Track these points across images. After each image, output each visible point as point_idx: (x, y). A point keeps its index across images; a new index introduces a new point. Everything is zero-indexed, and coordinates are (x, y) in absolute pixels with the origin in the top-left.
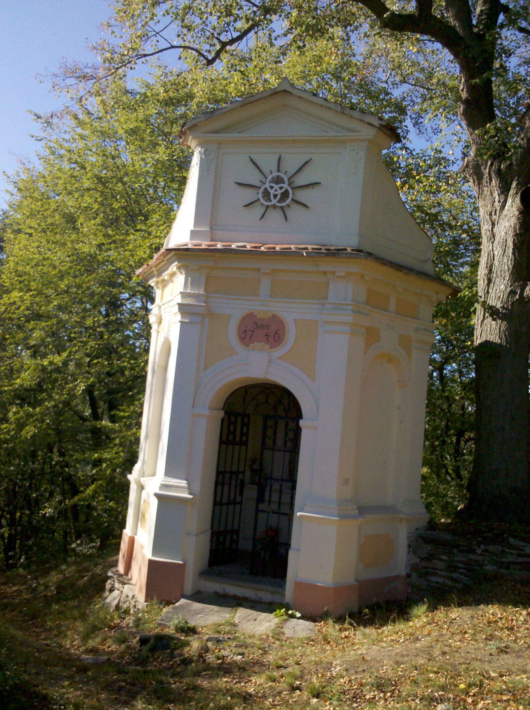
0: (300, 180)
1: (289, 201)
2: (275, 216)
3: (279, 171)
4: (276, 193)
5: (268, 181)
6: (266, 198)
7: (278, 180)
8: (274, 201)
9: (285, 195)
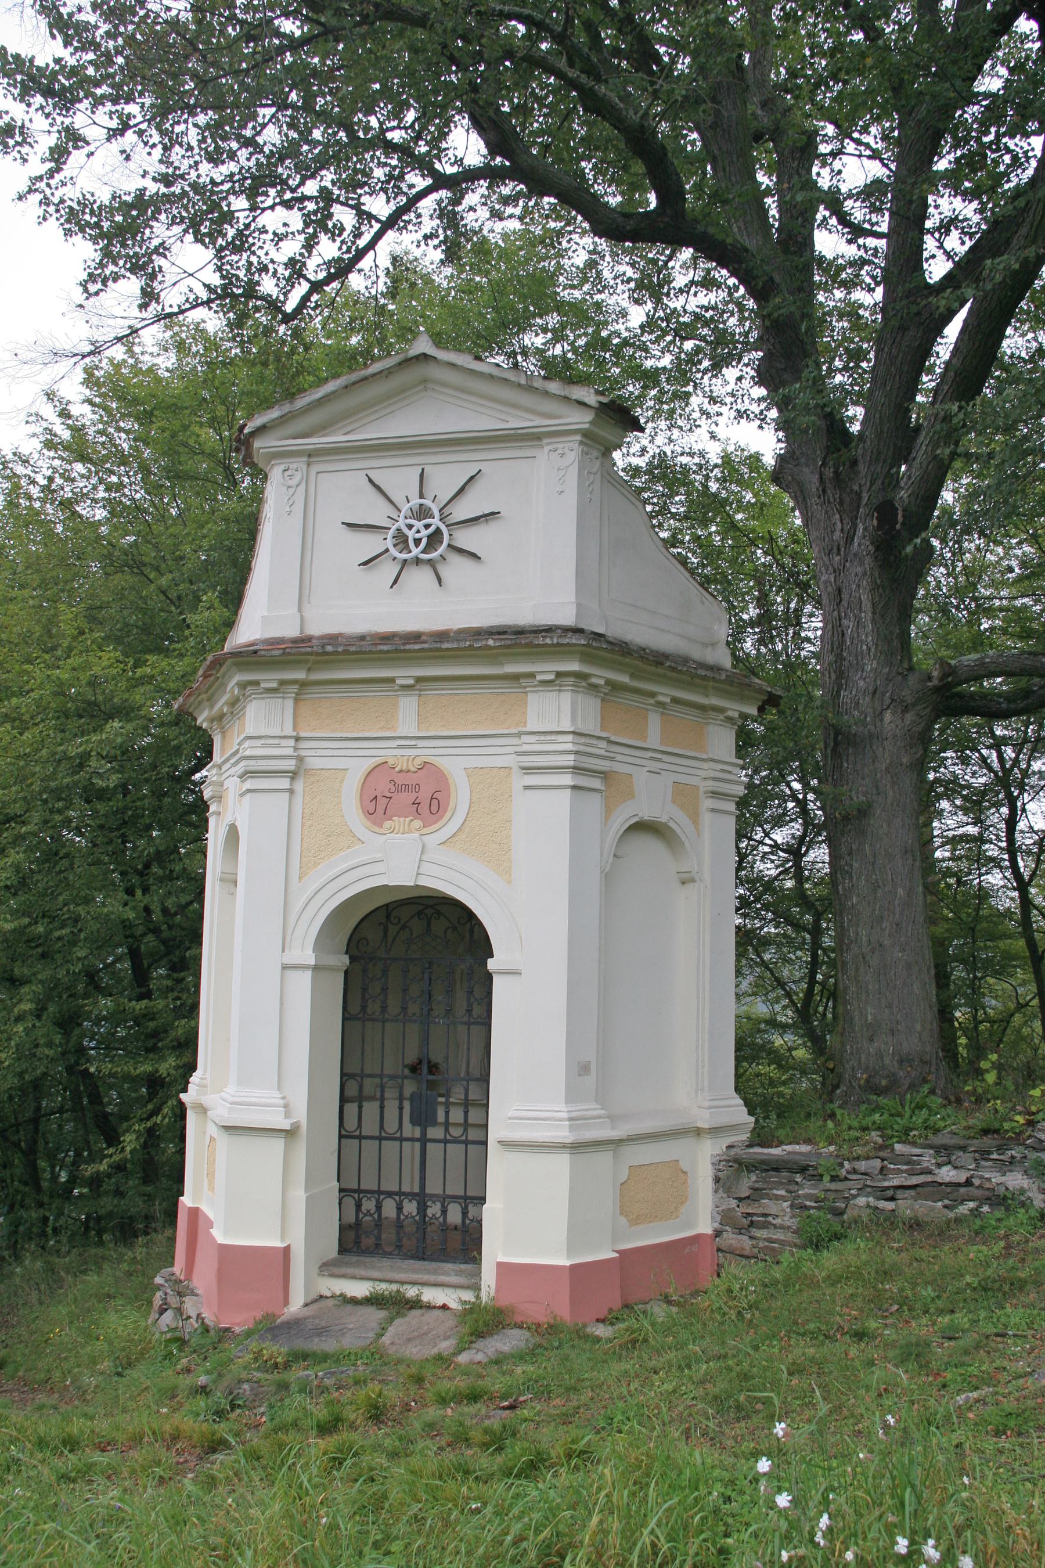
0: (462, 511)
1: (442, 549)
2: (422, 577)
3: (421, 496)
4: (418, 536)
5: (402, 515)
6: (401, 546)
7: (423, 513)
8: (415, 551)
9: (435, 538)
